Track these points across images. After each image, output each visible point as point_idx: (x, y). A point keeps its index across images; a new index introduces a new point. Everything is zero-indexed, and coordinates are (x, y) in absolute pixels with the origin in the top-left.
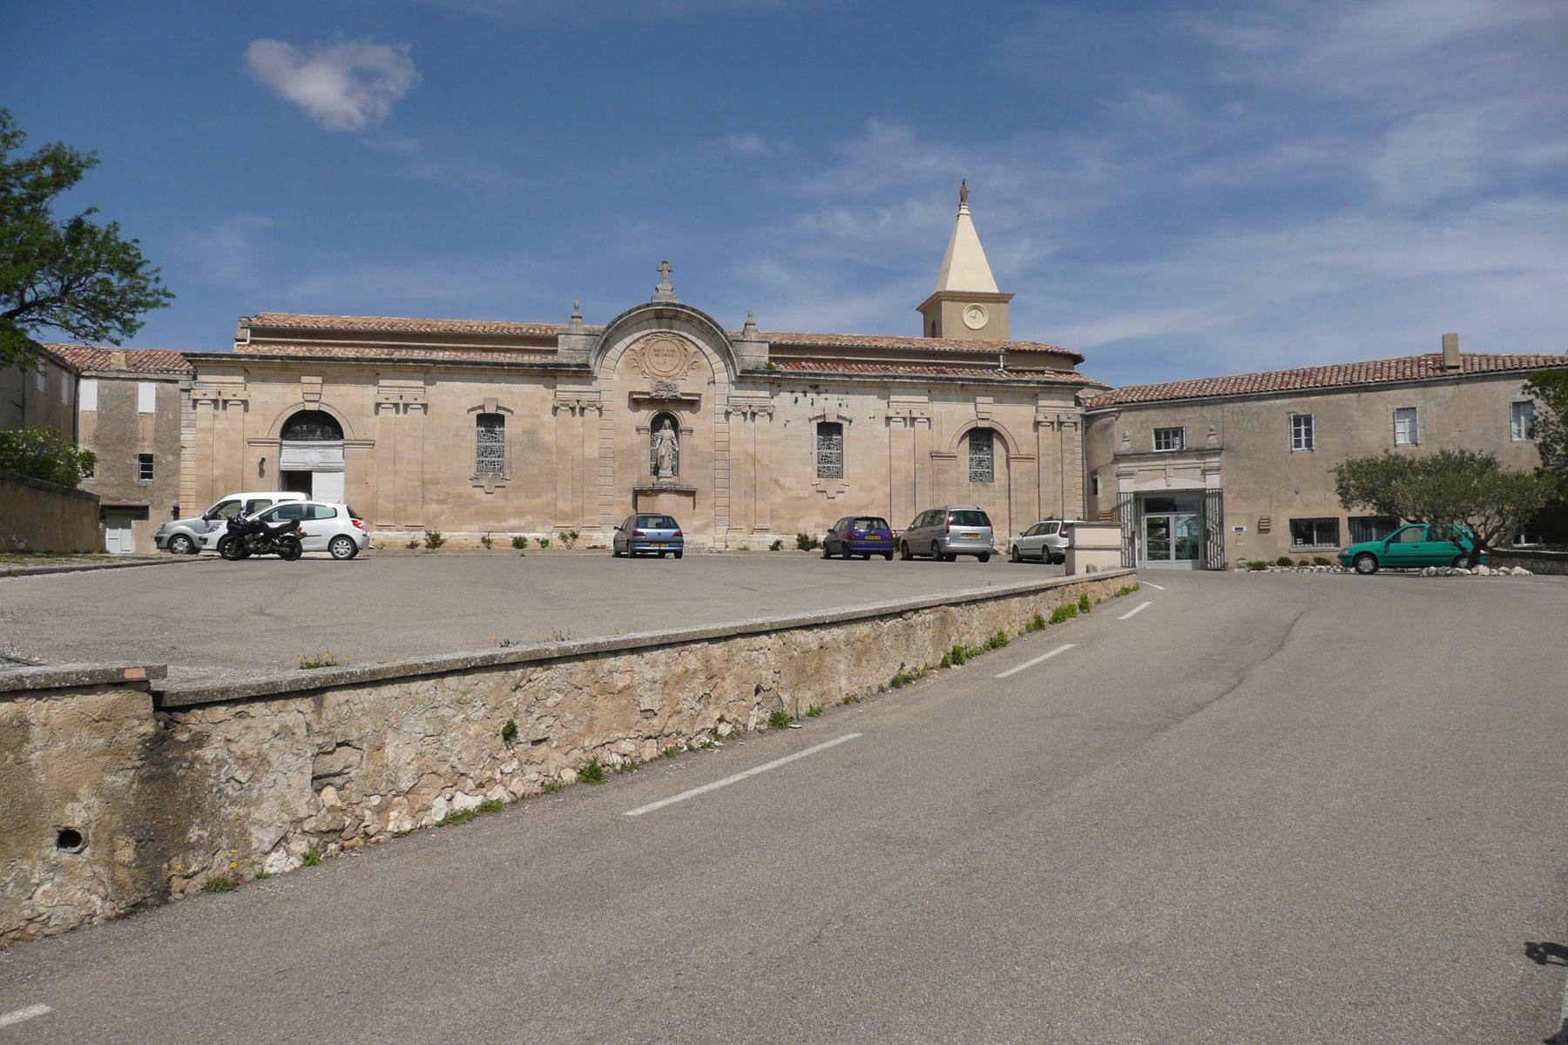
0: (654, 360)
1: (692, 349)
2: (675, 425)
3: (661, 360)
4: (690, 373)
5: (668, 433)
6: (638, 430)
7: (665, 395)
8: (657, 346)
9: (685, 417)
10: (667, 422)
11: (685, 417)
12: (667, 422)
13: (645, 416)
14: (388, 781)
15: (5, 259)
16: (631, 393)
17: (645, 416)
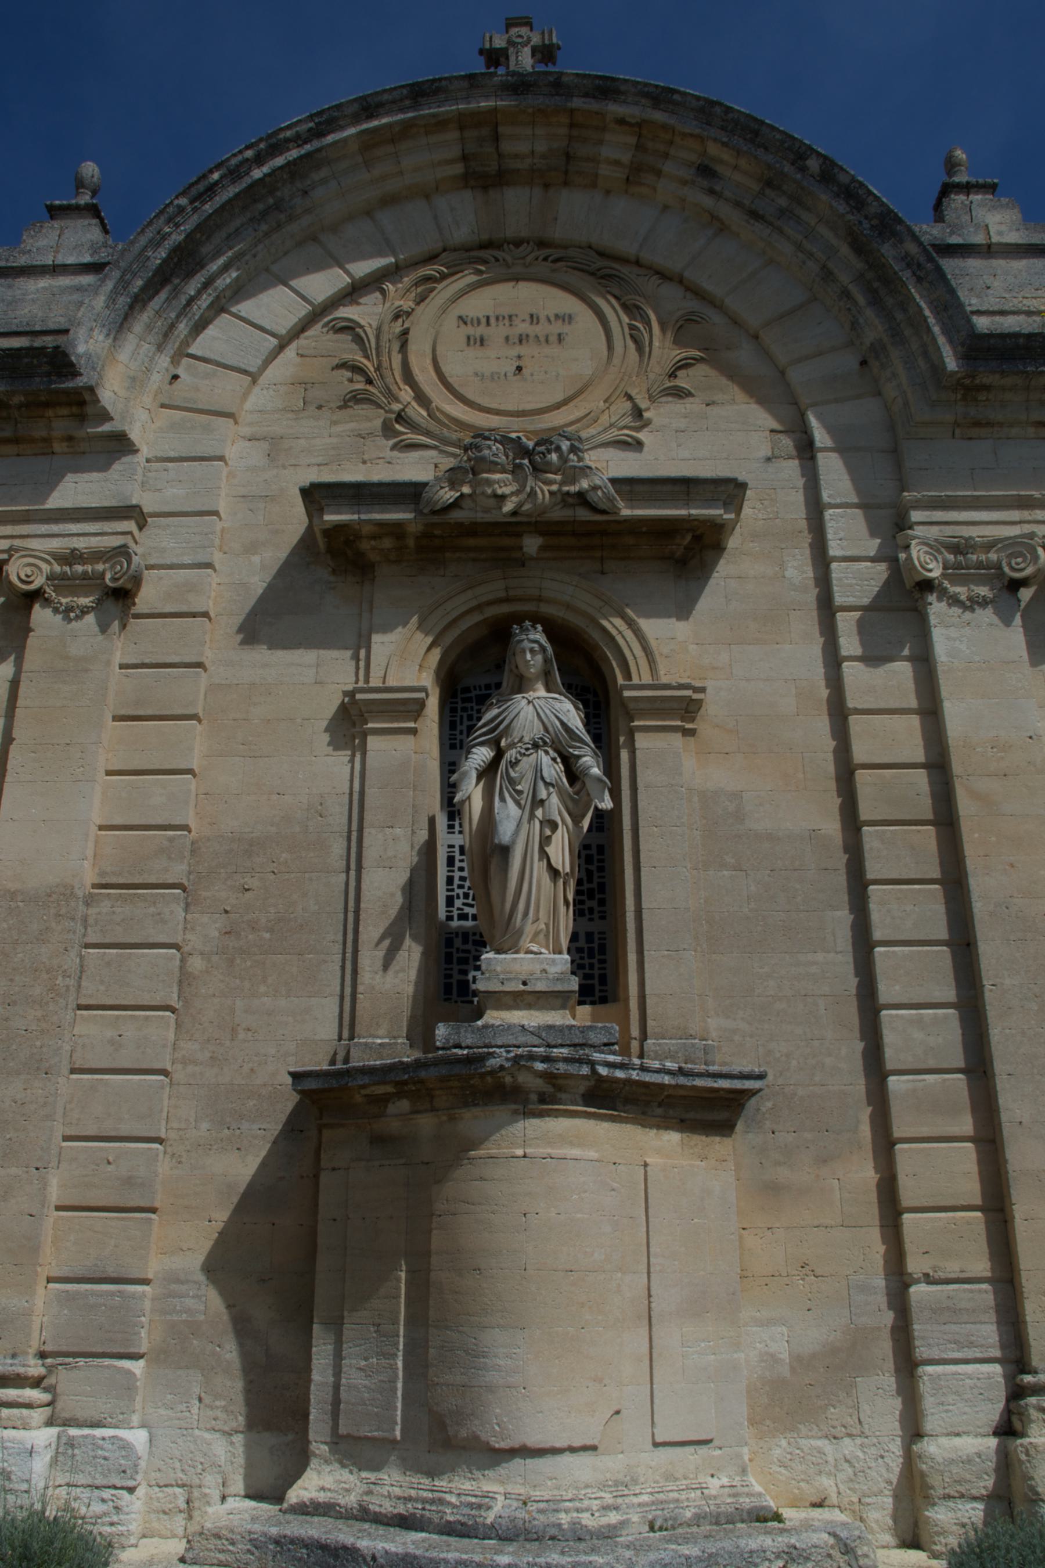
14: (466, 896)
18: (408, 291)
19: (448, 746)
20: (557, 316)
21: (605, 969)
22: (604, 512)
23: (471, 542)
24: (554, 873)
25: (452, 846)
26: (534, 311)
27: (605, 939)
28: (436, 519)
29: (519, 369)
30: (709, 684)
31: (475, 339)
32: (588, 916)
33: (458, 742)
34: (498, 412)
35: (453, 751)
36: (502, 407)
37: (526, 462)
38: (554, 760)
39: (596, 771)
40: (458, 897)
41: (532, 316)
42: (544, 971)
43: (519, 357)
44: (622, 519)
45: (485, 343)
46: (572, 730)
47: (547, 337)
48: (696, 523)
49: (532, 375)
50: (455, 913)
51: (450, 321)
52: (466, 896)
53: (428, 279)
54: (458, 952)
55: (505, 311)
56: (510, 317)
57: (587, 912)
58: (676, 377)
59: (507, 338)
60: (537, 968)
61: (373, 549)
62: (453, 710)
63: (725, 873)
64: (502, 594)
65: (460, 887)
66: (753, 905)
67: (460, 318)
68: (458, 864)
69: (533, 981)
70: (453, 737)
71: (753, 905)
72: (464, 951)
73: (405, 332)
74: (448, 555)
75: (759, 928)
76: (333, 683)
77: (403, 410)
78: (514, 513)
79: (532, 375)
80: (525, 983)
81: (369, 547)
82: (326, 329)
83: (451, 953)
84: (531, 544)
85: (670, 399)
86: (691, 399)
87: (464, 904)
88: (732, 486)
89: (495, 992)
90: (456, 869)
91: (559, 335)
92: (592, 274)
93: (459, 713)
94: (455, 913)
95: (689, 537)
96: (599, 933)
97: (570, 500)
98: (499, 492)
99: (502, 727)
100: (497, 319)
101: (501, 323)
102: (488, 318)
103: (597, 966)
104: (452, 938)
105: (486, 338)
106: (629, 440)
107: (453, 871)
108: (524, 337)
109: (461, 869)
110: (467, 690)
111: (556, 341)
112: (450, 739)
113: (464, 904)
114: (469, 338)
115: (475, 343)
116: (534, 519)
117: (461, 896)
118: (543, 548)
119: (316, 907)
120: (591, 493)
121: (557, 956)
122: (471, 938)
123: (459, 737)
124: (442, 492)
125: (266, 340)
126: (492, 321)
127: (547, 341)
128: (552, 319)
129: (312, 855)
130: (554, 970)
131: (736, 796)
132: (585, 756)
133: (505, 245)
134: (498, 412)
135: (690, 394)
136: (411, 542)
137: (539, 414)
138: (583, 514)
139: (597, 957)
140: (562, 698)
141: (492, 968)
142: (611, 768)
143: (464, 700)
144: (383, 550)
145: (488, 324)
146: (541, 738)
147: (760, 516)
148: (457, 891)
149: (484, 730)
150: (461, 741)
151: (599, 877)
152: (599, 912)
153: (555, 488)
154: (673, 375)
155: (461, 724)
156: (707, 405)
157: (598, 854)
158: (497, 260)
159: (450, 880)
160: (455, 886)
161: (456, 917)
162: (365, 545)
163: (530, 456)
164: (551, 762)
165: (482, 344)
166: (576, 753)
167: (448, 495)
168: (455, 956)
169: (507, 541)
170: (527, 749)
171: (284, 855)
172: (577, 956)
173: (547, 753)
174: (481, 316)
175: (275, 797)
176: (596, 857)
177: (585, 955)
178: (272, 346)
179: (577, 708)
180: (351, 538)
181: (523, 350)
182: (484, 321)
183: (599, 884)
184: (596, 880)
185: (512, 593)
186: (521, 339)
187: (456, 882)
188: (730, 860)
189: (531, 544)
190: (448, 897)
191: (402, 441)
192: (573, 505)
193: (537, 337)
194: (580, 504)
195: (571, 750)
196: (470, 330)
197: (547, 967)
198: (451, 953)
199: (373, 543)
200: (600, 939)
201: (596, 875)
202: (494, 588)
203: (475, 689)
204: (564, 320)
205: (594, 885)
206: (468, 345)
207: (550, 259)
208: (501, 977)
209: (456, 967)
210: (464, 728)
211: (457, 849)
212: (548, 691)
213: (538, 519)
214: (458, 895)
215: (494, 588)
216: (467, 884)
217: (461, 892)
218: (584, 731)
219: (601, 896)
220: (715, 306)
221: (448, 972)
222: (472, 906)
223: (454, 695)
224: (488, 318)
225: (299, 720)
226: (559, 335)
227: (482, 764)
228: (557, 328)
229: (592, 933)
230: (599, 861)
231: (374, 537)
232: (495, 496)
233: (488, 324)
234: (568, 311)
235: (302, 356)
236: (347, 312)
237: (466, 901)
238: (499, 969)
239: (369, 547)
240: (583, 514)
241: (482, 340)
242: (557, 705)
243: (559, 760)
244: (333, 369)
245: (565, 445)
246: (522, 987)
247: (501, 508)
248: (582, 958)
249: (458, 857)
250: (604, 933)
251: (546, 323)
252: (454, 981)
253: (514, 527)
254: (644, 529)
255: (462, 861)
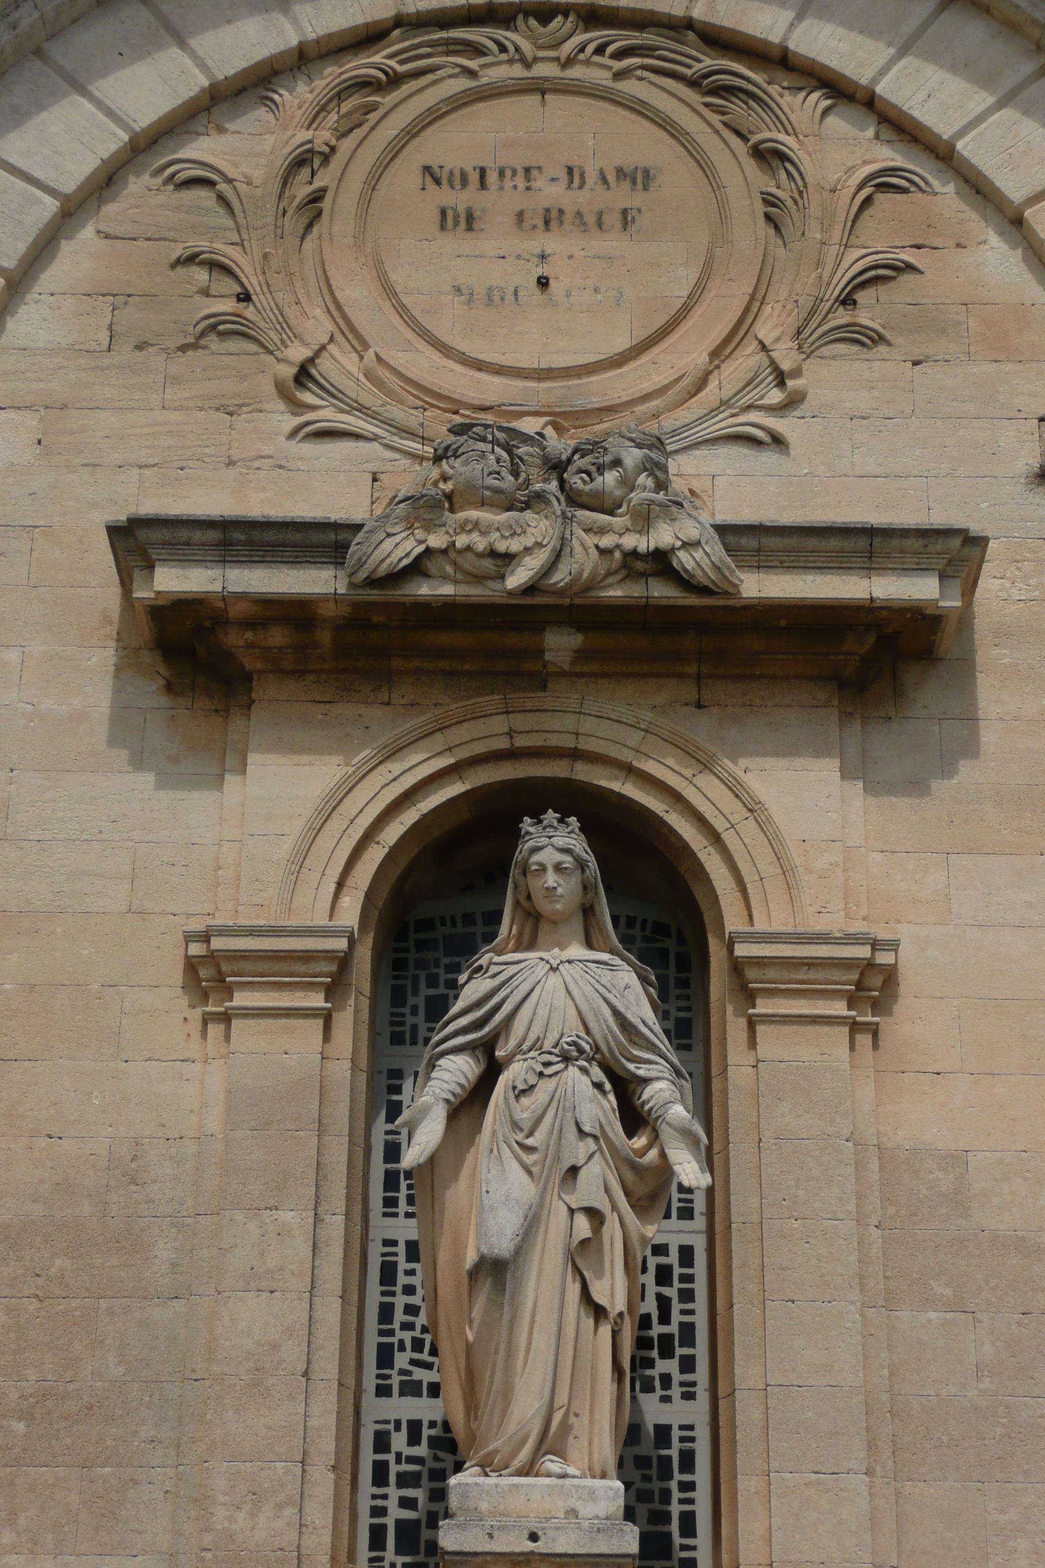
0: (430, 267)
1: (839, 152)
2: (657, 900)
3: (497, 257)
4: (834, 379)
5: (561, 983)
6: (212, 975)
7: (534, 547)
8: (455, 144)
9: (789, 822)
10: (554, 851)
11: (789, 822)
12: (554, 851)
13: (302, 818)
14: (418, 1345)
15: (1041, 1417)
16: (135, 541)
17: (302, 818)
18: (323, 108)
19: (387, 1037)
20: (621, 173)
21: (691, 1501)
22: (703, 590)
23: (444, 639)
24: (599, 1312)
25: (394, 1243)
26: (575, 161)
27: (692, 1440)
28: (375, 595)
29: (543, 283)
30: (904, 932)
31: (456, 217)
32: (659, 1393)
33: (407, 1028)
34: (499, 370)
35: (397, 1049)
36: (508, 361)
37: (553, 486)
38: (598, 1086)
39: (678, 1112)
40: (402, 1348)
41: (570, 170)
42: (572, 1513)
43: (543, 257)
44: (743, 602)
45: (476, 225)
46: (635, 1028)
47: (600, 214)
48: (885, 613)
49: (568, 295)
50: (395, 1380)
51: (405, 176)
52: (418, 1345)
53: (364, 84)
54: (398, 1461)
55: (518, 159)
56: (527, 170)
57: (657, 1383)
58: (855, 303)
59: (520, 216)
60: (561, 1505)
61: (250, 646)
62: (399, 965)
63: (933, 1315)
64: (501, 744)
65: (407, 1326)
66: (986, 1383)
67: (427, 169)
68: (402, 1280)
69: (550, 1533)
70: (397, 1021)
71: (986, 1383)
72: (411, 1460)
73: (317, 197)
74: (396, 663)
75: (999, 1430)
76: (164, 913)
77: (311, 360)
78: (530, 589)
79: (568, 295)
80: (534, 1537)
81: (241, 643)
82: (159, 180)
83: (386, 1463)
84: (561, 644)
85: (842, 348)
86: (883, 349)
87: (413, 1362)
88: (956, 542)
89: (476, 1554)
90: (398, 1289)
91: (625, 212)
92: (693, 83)
93: (412, 971)
94: (395, 1380)
95: (871, 639)
96: (682, 1428)
97: (640, 565)
98: (501, 547)
99: (498, 1017)
100: (502, 174)
101: (508, 183)
102: (483, 172)
103: (676, 1495)
104: (388, 1433)
105: (477, 214)
106: (760, 434)
107: (393, 1294)
108: (554, 214)
109: (409, 1290)
110: (426, 924)
111: (619, 226)
112: (392, 1024)
113: (413, 1362)
114: (443, 213)
115: (456, 223)
116: (567, 601)
117: (408, 1345)
118: (581, 655)
119: (121, 1370)
120: (682, 555)
121: (598, 1483)
122: (426, 1432)
123: (410, 1020)
124: (388, 544)
125: (38, 202)
126: (492, 177)
127: (600, 225)
128: (611, 178)
129: (115, 1261)
130: (588, 1510)
131: (956, 1160)
132: (658, 1079)
133: (520, 18)
134: (499, 370)
135: (879, 339)
136: (325, 637)
137: (579, 376)
138: (661, 591)
139: (677, 1476)
140: (618, 961)
141: (471, 1504)
142: (706, 1105)
143: (421, 946)
144: (269, 648)
145: (483, 185)
146: (574, 1044)
147: (1015, 594)
148: (400, 1334)
149: (463, 1021)
150: (414, 1028)
151: (683, 1312)
152: (682, 1384)
153: (606, 542)
154: (847, 301)
155: (415, 993)
156: (916, 363)
157: (682, 1265)
158: (503, 49)
159: (386, 1313)
160: (396, 1325)
161: (396, 1390)
162: (234, 639)
163: (566, 480)
164: (592, 1091)
165: (470, 228)
166: (641, 1072)
167: (398, 548)
168: (394, 1469)
169: (513, 639)
170: (547, 1064)
171: (58, 1262)
172: (636, 1475)
173: (584, 1070)
174: (469, 169)
175: (42, 1142)
176: (677, 1271)
177: (654, 1472)
178: (47, 216)
179: (643, 979)
180: (207, 623)
181: (551, 243)
182: (474, 177)
183: (682, 1325)
184: (676, 1317)
185: (521, 742)
186: (549, 219)
187: (399, 1316)
188: (939, 1288)
189: (561, 644)
190: (380, 1346)
191: (307, 424)
192: (643, 575)
193: (579, 214)
194: (656, 574)
195: (631, 1067)
196: (447, 197)
197: (579, 1506)
198: (386, 1463)
199: (249, 635)
200: (682, 1439)
201: (676, 1307)
202: (490, 731)
203: (443, 924)
204: (634, 182)
205: (673, 1328)
206: (443, 228)
207: (610, 49)
208: (488, 1523)
209: (394, 1493)
210: (420, 1001)
211: (401, 1249)
212: (589, 945)
213: (577, 601)
214: (401, 1342)
215: (490, 731)
216: (421, 1320)
217: (407, 1336)
218: (657, 1028)
219: (686, 1351)
220: (938, 157)
221: (379, 1503)
222: (429, 1366)
223: (401, 935)
224: (483, 172)
225: (95, 987)
226: (625, 212)
227: (458, 1090)
228: (621, 196)
229: (668, 1428)
230: (684, 1279)
231: (250, 623)
232: (493, 554)
233: (483, 185)
234: (642, 164)
235: (107, 236)
236: (202, 149)
237: (416, 1356)
238: (484, 1506)
239: (241, 643)
240: (661, 591)
241: (470, 218)
242: (606, 976)
243: (608, 1086)
244: (173, 266)
245: (632, 456)
246: (529, 1546)
247: (503, 577)
248: (647, 1478)
249: (403, 1265)
250: (691, 1428)
251: (600, 188)
252: (390, 1521)
253: (532, 613)
254: (783, 623)
255: (411, 1273)
